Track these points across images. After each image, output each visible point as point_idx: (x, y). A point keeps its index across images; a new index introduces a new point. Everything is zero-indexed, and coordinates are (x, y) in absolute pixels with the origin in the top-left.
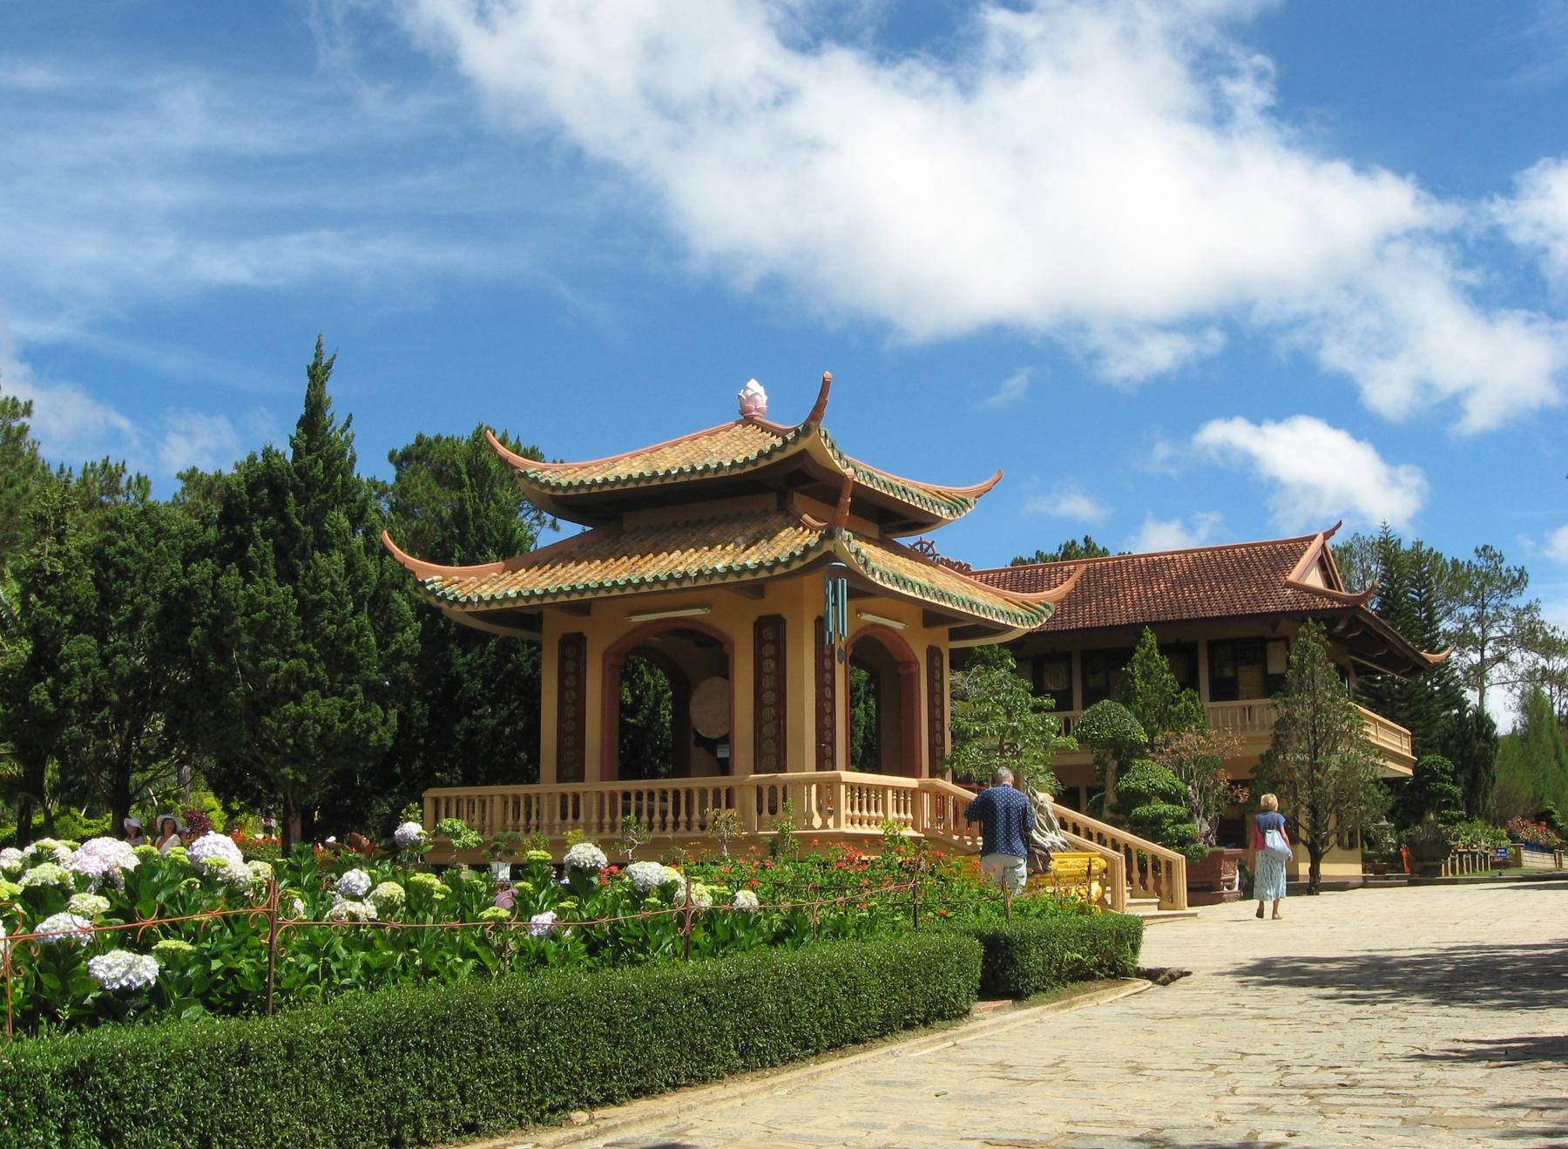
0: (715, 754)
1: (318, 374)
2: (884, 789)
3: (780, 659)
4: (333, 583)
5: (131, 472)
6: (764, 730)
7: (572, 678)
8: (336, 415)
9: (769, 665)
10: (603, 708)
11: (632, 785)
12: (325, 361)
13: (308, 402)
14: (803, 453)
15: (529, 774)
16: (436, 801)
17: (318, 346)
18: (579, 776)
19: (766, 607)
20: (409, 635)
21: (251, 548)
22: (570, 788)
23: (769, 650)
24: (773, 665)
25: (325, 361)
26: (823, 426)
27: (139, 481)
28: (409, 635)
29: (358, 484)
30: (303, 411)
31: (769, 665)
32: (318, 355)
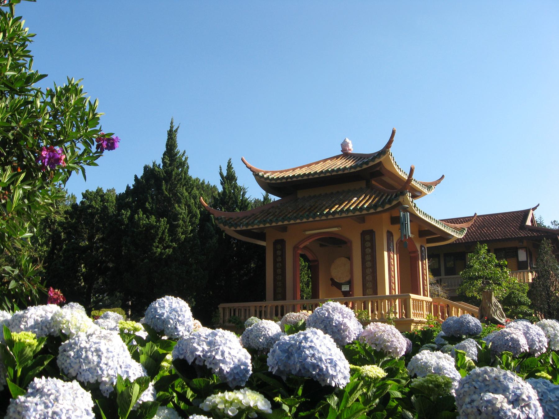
0: (340, 289)
1: (171, 135)
2: (423, 301)
3: (373, 248)
4: (183, 217)
5: (70, 193)
6: (367, 278)
7: (280, 258)
8: (180, 147)
9: (368, 251)
10: (513, 212)
11: (447, 277)
12: (174, 129)
13: (167, 145)
14: (380, 163)
15: (262, 298)
16: (224, 309)
17: (172, 123)
18: (284, 298)
19: (366, 226)
20: (215, 240)
21: (147, 204)
22: (280, 303)
23: (368, 244)
24: (370, 251)
25: (174, 129)
26: (391, 150)
27: (72, 197)
28: (215, 240)
29: (190, 178)
30: (165, 149)
31: (368, 251)
32: (172, 127)
